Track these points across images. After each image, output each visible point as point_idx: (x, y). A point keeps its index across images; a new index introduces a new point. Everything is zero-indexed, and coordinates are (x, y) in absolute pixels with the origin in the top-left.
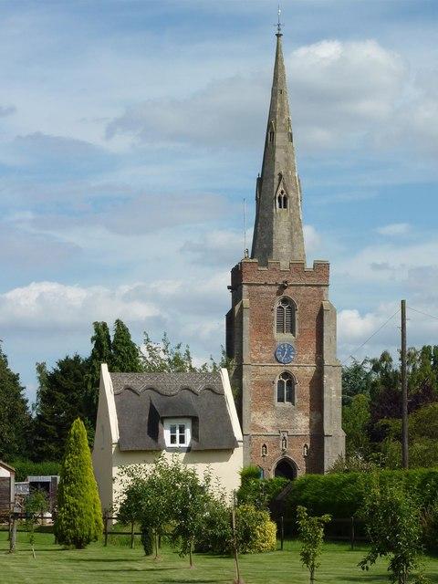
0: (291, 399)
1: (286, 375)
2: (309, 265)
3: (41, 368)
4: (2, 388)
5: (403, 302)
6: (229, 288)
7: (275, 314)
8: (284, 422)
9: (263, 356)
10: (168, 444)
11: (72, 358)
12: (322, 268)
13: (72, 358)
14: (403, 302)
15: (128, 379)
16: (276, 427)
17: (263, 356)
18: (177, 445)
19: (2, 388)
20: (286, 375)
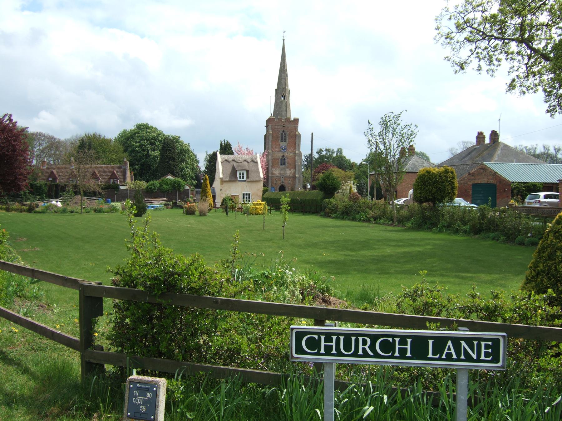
0: (284, 164)
1: (283, 156)
2: (292, 119)
3: (27, 128)
4: (561, 283)
5: (312, 133)
6: (179, 137)
7: (280, 136)
8: (282, 172)
9: (276, 150)
10: (239, 179)
11: (352, 162)
12: (296, 120)
13: (352, 162)
14: (312, 133)
15: (226, 157)
16: (280, 174)
17: (276, 150)
18: (242, 179)
19: (561, 283)
20: (283, 156)
